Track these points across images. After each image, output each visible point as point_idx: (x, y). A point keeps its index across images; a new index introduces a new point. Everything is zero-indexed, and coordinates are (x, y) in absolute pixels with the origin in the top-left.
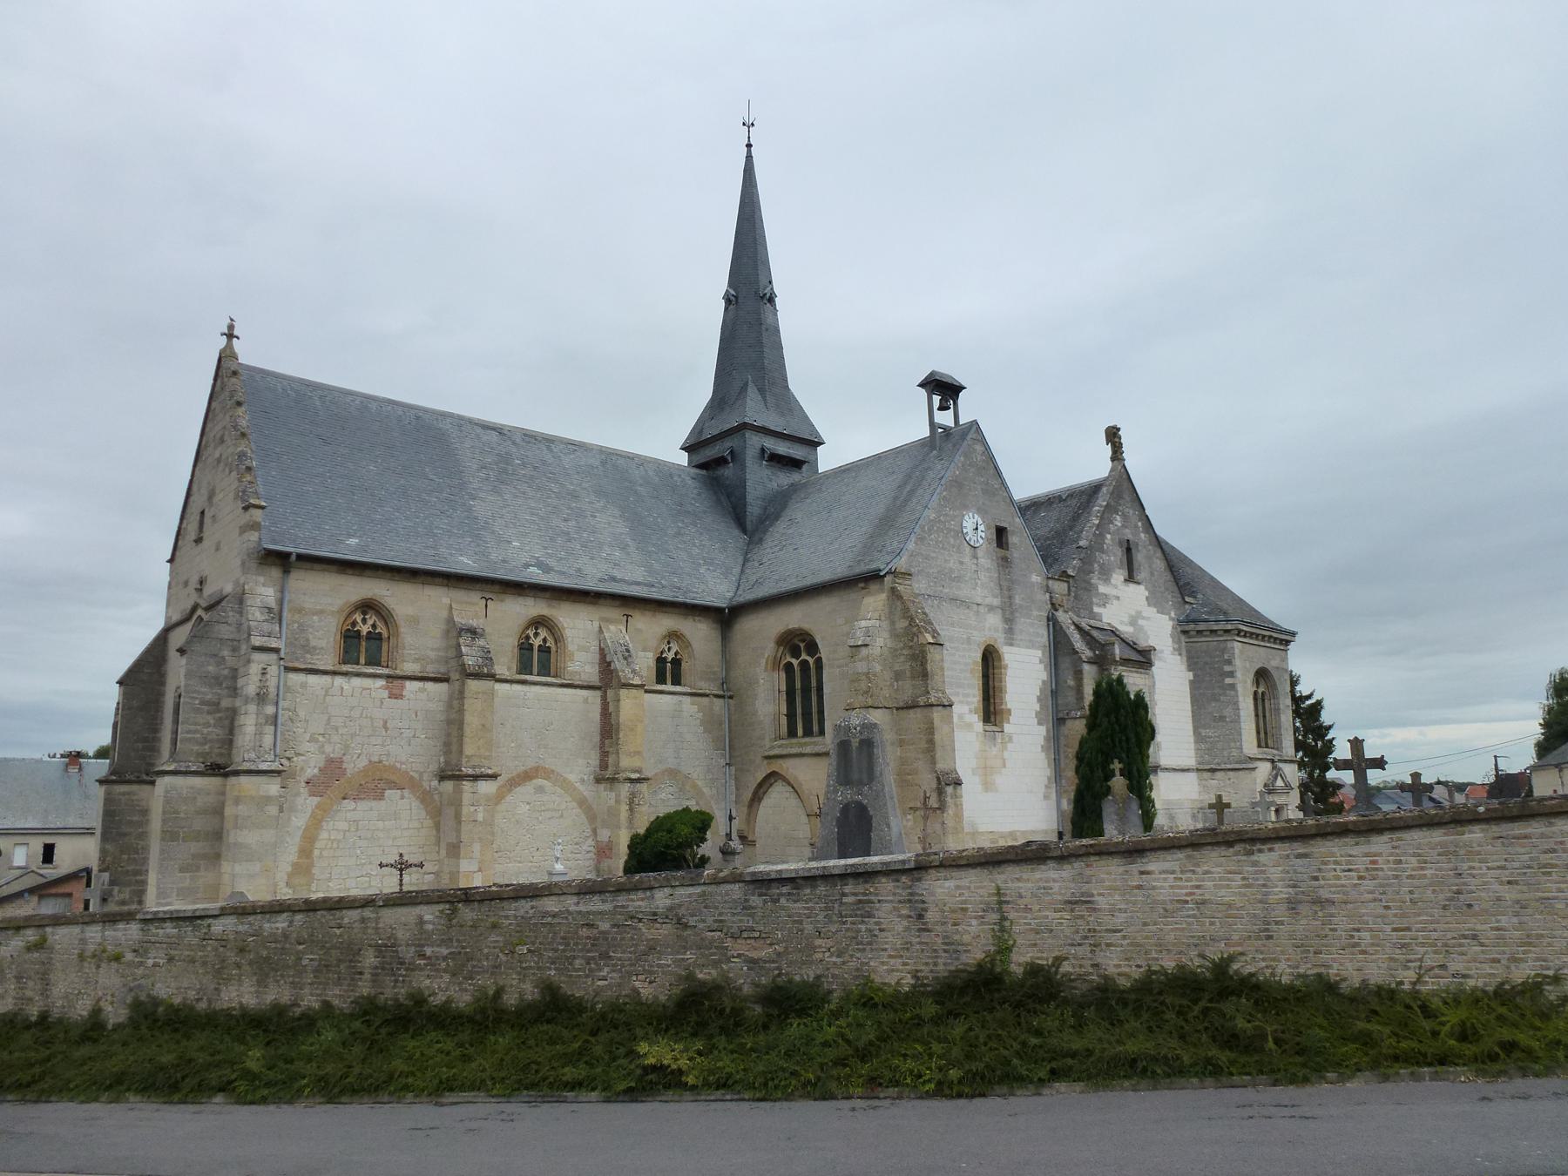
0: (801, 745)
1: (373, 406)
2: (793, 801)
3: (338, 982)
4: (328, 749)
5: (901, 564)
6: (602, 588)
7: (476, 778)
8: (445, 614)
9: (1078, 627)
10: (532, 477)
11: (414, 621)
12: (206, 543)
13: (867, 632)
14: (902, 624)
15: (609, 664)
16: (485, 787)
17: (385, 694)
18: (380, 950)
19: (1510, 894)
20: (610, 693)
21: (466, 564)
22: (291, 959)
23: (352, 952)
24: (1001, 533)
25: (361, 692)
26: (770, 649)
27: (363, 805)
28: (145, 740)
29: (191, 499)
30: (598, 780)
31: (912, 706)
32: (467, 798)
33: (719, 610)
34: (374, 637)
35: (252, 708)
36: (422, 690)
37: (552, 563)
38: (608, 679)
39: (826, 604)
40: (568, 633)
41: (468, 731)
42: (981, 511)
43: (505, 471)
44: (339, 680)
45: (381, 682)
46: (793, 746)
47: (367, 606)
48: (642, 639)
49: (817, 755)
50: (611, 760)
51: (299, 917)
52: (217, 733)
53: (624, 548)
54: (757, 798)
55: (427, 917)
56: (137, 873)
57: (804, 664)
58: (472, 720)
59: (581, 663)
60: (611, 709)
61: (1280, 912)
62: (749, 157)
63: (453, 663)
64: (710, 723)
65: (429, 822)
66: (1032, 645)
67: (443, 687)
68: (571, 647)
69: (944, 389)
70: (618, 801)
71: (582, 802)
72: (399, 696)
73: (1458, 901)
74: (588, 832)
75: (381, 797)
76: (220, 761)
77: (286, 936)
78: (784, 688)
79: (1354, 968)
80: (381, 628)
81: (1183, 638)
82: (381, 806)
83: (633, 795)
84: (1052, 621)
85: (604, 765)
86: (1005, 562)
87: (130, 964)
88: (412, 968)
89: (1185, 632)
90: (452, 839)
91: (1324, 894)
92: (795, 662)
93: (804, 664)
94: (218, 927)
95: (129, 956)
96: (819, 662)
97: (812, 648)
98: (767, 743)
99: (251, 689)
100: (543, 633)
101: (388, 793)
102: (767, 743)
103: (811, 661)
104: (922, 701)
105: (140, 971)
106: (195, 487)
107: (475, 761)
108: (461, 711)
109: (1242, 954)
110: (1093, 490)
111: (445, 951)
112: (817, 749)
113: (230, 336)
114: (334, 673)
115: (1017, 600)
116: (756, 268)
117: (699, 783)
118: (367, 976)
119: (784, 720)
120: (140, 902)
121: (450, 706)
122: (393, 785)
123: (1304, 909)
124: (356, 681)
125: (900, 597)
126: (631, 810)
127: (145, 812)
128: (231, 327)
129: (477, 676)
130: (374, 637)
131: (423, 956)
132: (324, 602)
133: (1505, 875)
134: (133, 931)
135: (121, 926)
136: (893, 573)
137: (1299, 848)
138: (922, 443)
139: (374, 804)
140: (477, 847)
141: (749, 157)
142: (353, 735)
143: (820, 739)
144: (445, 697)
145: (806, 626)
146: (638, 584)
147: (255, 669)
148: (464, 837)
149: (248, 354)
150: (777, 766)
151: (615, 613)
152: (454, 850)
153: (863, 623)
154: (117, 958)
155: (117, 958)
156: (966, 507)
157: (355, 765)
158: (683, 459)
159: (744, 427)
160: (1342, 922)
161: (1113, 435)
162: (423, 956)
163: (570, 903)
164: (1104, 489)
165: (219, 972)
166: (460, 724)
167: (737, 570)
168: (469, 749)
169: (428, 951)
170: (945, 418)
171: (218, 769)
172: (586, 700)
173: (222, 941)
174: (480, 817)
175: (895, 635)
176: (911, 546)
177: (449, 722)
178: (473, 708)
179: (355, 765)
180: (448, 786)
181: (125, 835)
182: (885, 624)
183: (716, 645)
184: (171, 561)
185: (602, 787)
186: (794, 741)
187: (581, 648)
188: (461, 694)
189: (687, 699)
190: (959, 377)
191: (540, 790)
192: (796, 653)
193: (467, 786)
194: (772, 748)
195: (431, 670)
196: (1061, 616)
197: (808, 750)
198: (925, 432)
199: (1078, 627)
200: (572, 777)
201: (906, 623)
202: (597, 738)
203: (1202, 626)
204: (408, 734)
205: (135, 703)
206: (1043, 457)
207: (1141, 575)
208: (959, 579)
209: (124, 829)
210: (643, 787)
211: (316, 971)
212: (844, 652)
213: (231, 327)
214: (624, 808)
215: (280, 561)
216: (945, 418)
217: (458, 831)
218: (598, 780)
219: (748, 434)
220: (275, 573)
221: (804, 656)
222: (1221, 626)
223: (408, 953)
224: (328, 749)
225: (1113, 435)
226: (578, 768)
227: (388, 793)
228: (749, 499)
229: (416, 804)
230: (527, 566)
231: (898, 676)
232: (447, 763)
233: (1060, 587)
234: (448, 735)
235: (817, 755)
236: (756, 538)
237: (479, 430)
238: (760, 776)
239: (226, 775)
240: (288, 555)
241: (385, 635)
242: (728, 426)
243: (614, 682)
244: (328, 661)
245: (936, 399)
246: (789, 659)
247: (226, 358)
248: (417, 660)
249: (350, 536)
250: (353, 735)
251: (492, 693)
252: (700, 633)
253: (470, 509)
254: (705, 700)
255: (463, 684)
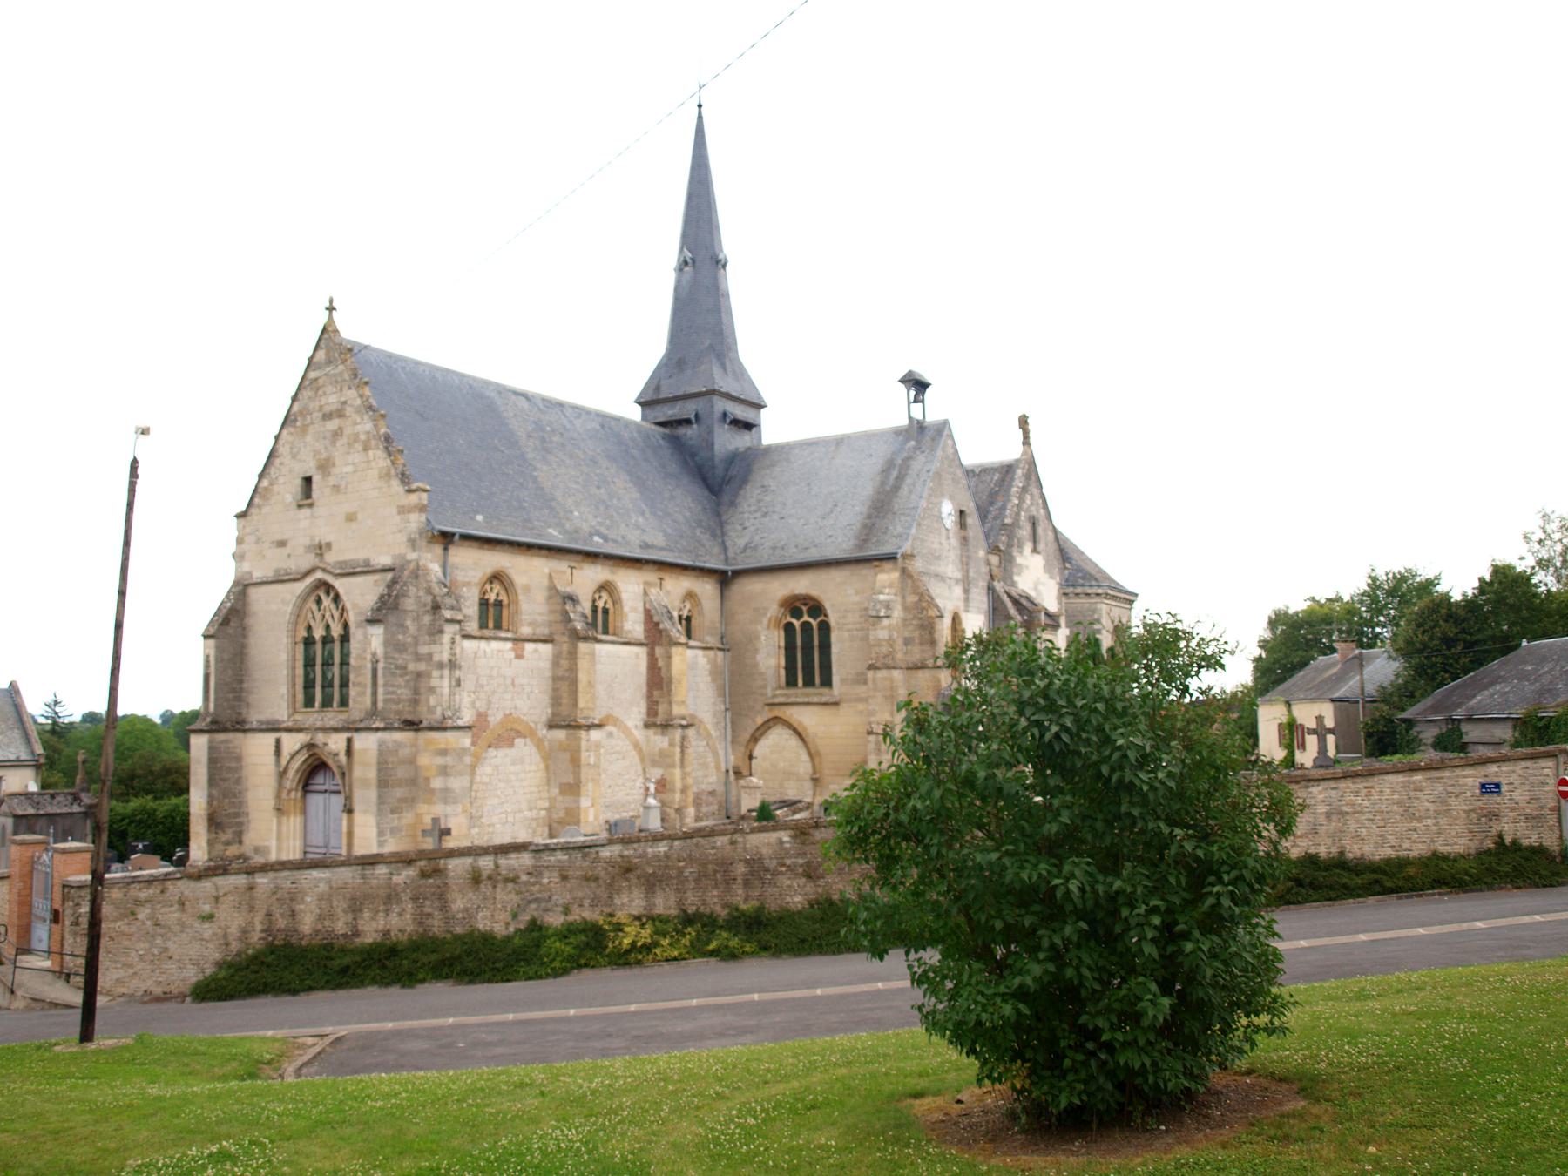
0: (808, 695)
1: (438, 375)
2: (794, 742)
3: (716, 886)
4: (478, 704)
5: (906, 547)
6: (637, 554)
7: (590, 727)
8: (546, 582)
9: (1009, 596)
10: (563, 445)
11: (527, 589)
12: (319, 510)
13: (888, 606)
14: (912, 599)
15: (657, 624)
16: (595, 735)
17: (512, 655)
18: (747, 861)
19: (1432, 807)
20: (659, 651)
21: (555, 537)
22: (674, 873)
23: (725, 865)
24: (962, 512)
25: (490, 654)
26: (774, 610)
27: (502, 752)
28: (234, 690)
29: (277, 461)
30: (647, 726)
31: (921, 666)
32: (583, 743)
33: (724, 573)
34: (498, 604)
35: (446, 672)
36: (536, 651)
37: (603, 530)
38: (655, 636)
39: (837, 575)
40: (624, 596)
41: (581, 687)
42: (952, 498)
43: (543, 440)
44: (483, 644)
45: (509, 645)
46: (800, 694)
47: (497, 577)
48: (673, 591)
49: (825, 704)
50: (662, 709)
51: (677, 843)
52: (405, 693)
53: (643, 513)
54: (755, 739)
55: (786, 839)
56: (237, 815)
57: (806, 626)
58: (582, 677)
59: (634, 624)
60: (661, 663)
61: (1322, 818)
62: (700, 117)
63: (560, 627)
64: (715, 673)
65: (542, 766)
66: (979, 612)
67: (546, 649)
68: (626, 609)
69: (918, 385)
70: (672, 744)
71: (636, 746)
72: (519, 656)
73: (1409, 814)
74: (640, 768)
75: (511, 745)
76: (409, 717)
77: (667, 855)
78: (782, 644)
79: (1354, 850)
80: (503, 597)
81: (1064, 599)
82: (511, 752)
83: (683, 738)
84: (991, 589)
85: (652, 711)
86: (964, 540)
87: (527, 883)
88: (775, 873)
89: (1065, 594)
90: (570, 779)
91: (1345, 809)
92: (794, 621)
93: (806, 626)
94: (605, 853)
95: (524, 878)
96: (825, 628)
97: (816, 609)
98: (769, 691)
99: (445, 657)
100: (605, 596)
101: (517, 741)
102: (769, 691)
103: (814, 623)
104: (930, 663)
105: (537, 887)
106: (283, 450)
107: (586, 713)
108: (573, 669)
109: (269, 914)
110: (1007, 470)
111: (801, 861)
112: (824, 699)
113: (331, 309)
114: (481, 638)
115: (972, 574)
116: (711, 233)
117: (709, 726)
118: (739, 881)
119: (783, 672)
120: (240, 842)
121: (555, 664)
122: (519, 734)
123: (1334, 817)
124: (495, 645)
125: (910, 576)
126: (682, 752)
127: (239, 759)
128: (331, 301)
129: (586, 639)
130: (498, 604)
131: (783, 865)
132: (472, 565)
133: (1431, 798)
134: (526, 859)
135: (513, 855)
136: (905, 556)
137: (1332, 784)
138: (898, 432)
139: (507, 751)
140: (590, 786)
141: (700, 117)
142: (494, 692)
143: (825, 690)
144: (550, 656)
145: (814, 593)
146: (662, 549)
147: (446, 638)
148: (583, 777)
149: (349, 331)
150: (777, 712)
151: (651, 576)
152: (572, 789)
153: (882, 597)
154: (514, 880)
155: (514, 880)
156: (942, 495)
157: (495, 718)
158: (635, 414)
159: (712, 392)
160: (1353, 825)
161: (1023, 422)
162: (783, 865)
163: (345, 829)
164: (1019, 472)
165: (610, 885)
166: (574, 682)
167: (718, 532)
168: (581, 704)
169: (788, 862)
170: (917, 411)
171: (412, 725)
172: (637, 656)
173: (610, 862)
174: (592, 761)
175: (906, 608)
176: (913, 531)
177: (555, 679)
178: (583, 664)
179: (495, 718)
180: (561, 734)
181: (224, 780)
182: (899, 599)
183: (718, 601)
184: (241, 516)
185: (651, 732)
186: (791, 691)
187: (634, 610)
188: (573, 655)
189: (700, 652)
190: (927, 377)
191: (610, 735)
192: (796, 613)
193: (583, 733)
194: (775, 696)
195: (544, 631)
196: (998, 586)
197: (816, 700)
198: (905, 422)
199: (1009, 596)
200: (630, 724)
201: (916, 599)
202: (644, 689)
203: (1079, 590)
204: (527, 689)
205: (226, 656)
206: (983, 443)
207: (1041, 547)
208: (938, 558)
209: (225, 775)
210: (691, 732)
211: (697, 880)
212: (853, 618)
213: (331, 301)
214: (678, 750)
215: (446, 538)
216: (917, 411)
217: (577, 774)
218: (647, 726)
219: (716, 399)
220: (438, 549)
221: (806, 618)
222: (1095, 590)
223: (772, 864)
224: (478, 704)
225: (1023, 422)
226: (634, 716)
227: (517, 741)
228: (717, 460)
229: (534, 750)
230: (591, 535)
231: (907, 642)
232: (553, 714)
233: (994, 560)
234: (555, 690)
235: (825, 704)
236: (725, 498)
237: (514, 397)
238: (759, 721)
239: (417, 730)
240: (453, 534)
241: (505, 601)
242: (695, 390)
243: (664, 641)
244: (473, 627)
245: (912, 393)
246: (789, 619)
247: (328, 332)
248: (530, 624)
249: (477, 512)
250: (494, 692)
251: (593, 654)
252: (707, 589)
253: (535, 480)
254: (711, 653)
255: (575, 647)
